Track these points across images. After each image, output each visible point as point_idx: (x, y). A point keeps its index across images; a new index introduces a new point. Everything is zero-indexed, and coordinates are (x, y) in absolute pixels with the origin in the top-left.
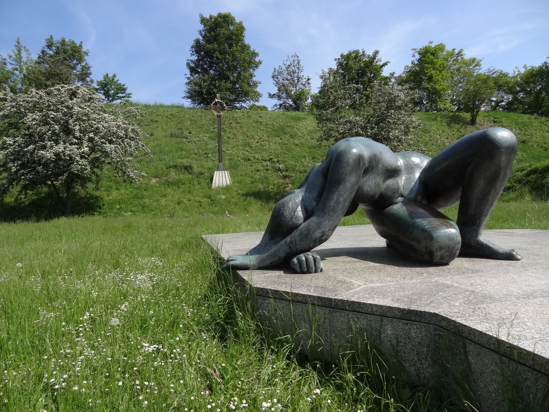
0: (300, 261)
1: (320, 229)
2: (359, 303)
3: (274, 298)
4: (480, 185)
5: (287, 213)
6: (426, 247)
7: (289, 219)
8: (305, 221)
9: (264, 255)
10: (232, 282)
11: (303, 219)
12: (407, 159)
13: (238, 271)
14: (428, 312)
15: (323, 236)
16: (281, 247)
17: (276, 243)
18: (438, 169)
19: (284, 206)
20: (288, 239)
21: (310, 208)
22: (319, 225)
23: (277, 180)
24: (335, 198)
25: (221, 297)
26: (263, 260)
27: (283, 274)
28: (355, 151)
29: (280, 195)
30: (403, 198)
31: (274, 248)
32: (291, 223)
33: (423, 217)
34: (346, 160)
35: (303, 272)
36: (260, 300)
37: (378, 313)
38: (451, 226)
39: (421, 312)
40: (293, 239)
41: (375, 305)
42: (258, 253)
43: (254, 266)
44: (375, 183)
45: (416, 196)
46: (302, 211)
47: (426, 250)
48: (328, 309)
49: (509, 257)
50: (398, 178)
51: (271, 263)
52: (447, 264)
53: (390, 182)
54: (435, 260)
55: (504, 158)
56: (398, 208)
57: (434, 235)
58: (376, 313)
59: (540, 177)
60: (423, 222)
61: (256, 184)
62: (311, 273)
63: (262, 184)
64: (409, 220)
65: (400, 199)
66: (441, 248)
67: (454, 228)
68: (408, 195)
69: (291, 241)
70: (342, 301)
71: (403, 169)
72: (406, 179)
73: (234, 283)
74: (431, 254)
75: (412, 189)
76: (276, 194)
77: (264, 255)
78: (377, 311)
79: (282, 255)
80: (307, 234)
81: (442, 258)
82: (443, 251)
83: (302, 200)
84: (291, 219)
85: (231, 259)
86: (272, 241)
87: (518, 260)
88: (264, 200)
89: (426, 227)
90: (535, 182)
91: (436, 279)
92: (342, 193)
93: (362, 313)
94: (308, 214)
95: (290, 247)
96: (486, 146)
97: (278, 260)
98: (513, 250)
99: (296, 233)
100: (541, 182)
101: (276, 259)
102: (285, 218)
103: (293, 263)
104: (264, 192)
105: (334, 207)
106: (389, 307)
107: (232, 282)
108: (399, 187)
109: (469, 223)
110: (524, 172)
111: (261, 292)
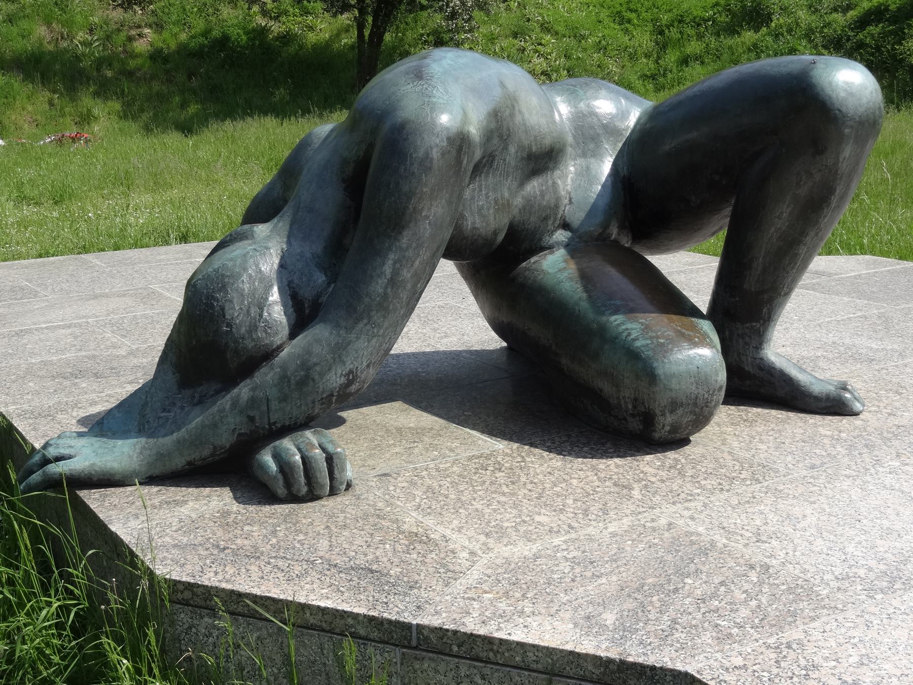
0: (285, 467)
1: (344, 363)
2: (488, 640)
3: (232, 613)
4: (780, 217)
5: (236, 311)
6: (636, 400)
7: (243, 330)
8: (293, 335)
9: (168, 441)
10: (78, 550)
11: (286, 332)
12: (582, 105)
13: (83, 494)
14: (671, 670)
15: (349, 383)
16: (220, 417)
17: (201, 402)
18: (668, 146)
19: (224, 288)
20: (243, 391)
21: (307, 293)
22: (339, 351)
23: (100, 13)
24: (388, 269)
25: (49, 604)
26: (161, 456)
27: (235, 507)
28: (444, 119)
29: (116, 65)
30: (568, 234)
31: (197, 420)
32: (250, 344)
33: (630, 310)
34: (421, 153)
35: (294, 498)
36: (184, 617)
37: (540, 666)
38: (703, 341)
39: (653, 668)
40: (260, 394)
41: (534, 646)
42: (143, 430)
43: (135, 474)
44: (496, 202)
45: (606, 225)
46: (284, 305)
47: (634, 407)
48: (398, 652)
49: (835, 406)
50: (557, 173)
51: (189, 463)
52: (685, 442)
53: (534, 186)
54: (657, 435)
55: (847, 151)
56: (554, 266)
57: (660, 371)
58: (534, 666)
59: (891, 33)
60: (629, 326)
61: (24, 24)
62: (319, 498)
63: (49, 24)
64: (591, 315)
65: (561, 236)
66: (674, 405)
67: (711, 346)
68: (582, 224)
69: (253, 402)
70: (440, 632)
71: (570, 139)
72: (579, 174)
73: (84, 552)
74: (648, 419)
75: (594, 205)
76: (100, 63)
77: (168, 441)
78: (537, 662)
79: (225, 439)
80: (303, 378)
81: (675, 428)
82: (680, 412)
83: (282, 266)
84: (250, 332)
85: (52, 452)
86: (187, 392)
87: (856, 414)
88: (60, 86)
89: (638, 344)
90: (878, 48)
91: (666, 514)
92: (410, 253)
93: (498, 664)
94: (303, 314)
95: (251, 419)
96: (803, 112)
97: (212, 455)
98: (844, 388)
99: (266, 376)
100: (894, 49)
101: (206, 452)
102: (229, 325)
103: (263, 467)
104: (57, 56)
105: (385, 296)
106: (572, 653)
107: (78, 550)
108: (558, 199)
109: (744, 307)
110: (851, 14)
111: (187, 595)
